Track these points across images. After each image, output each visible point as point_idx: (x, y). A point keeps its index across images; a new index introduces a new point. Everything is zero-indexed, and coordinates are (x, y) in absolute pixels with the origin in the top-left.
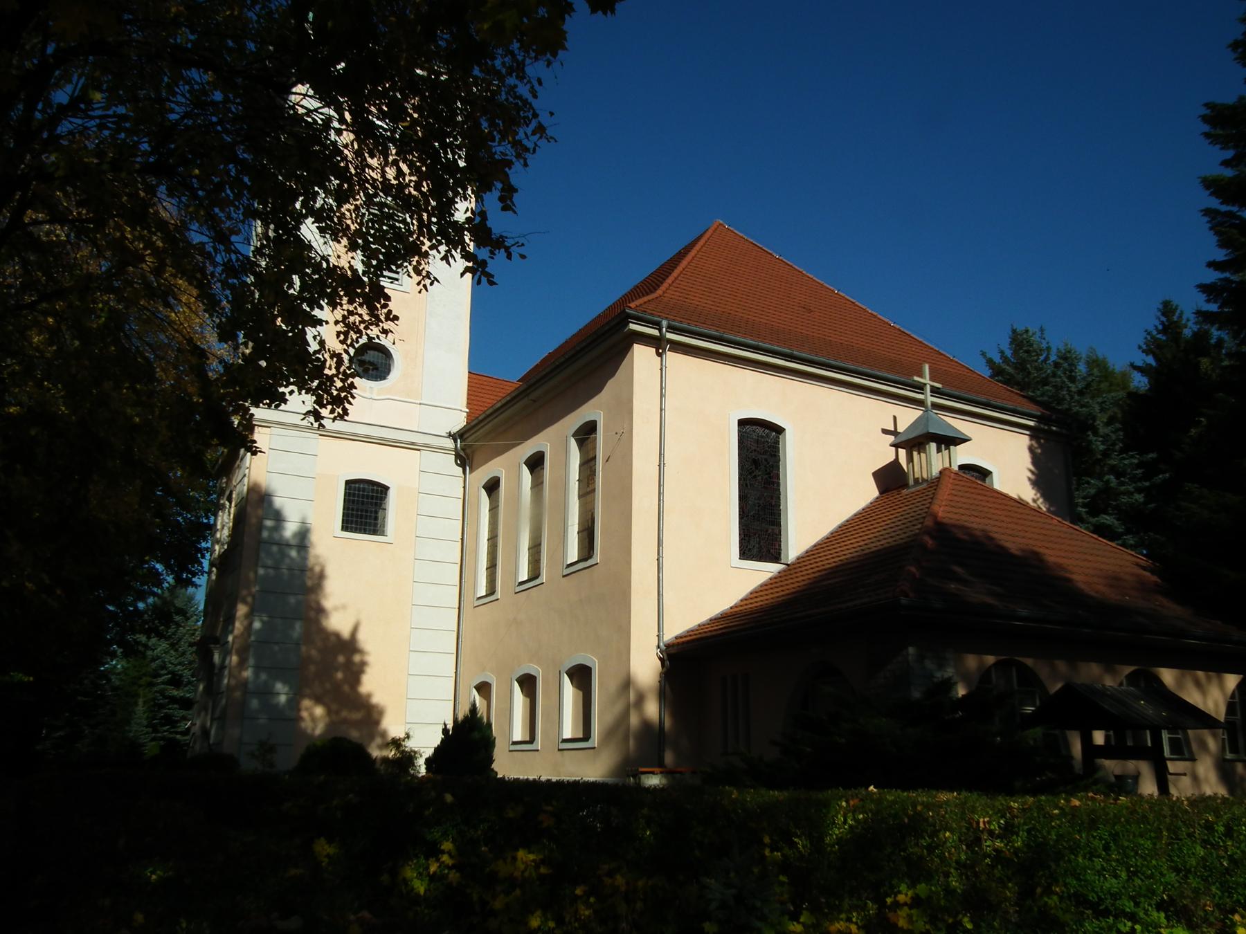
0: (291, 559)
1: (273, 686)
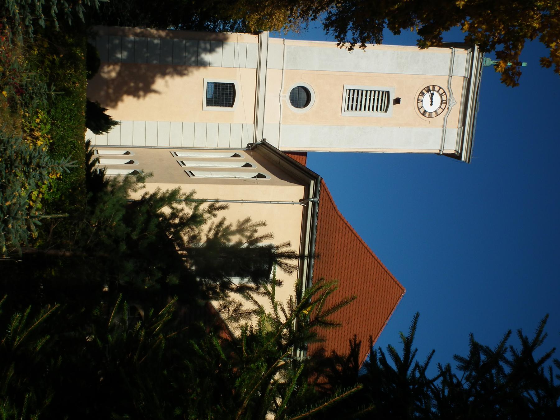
0: (190, 58)
1: (125, 51)
